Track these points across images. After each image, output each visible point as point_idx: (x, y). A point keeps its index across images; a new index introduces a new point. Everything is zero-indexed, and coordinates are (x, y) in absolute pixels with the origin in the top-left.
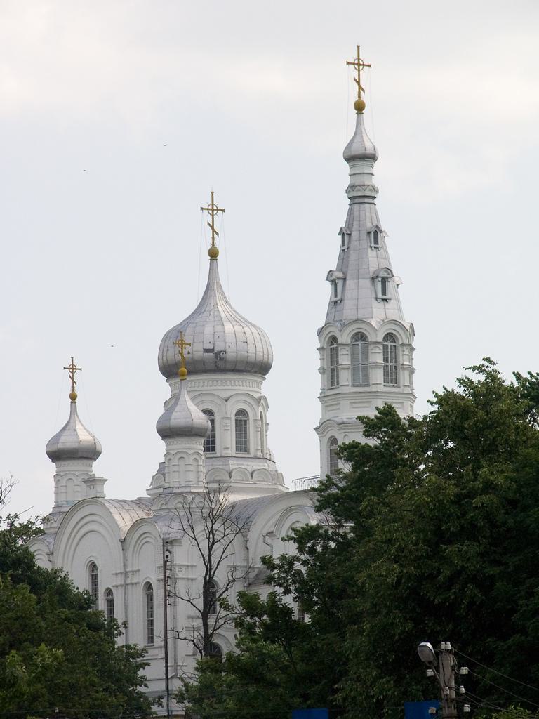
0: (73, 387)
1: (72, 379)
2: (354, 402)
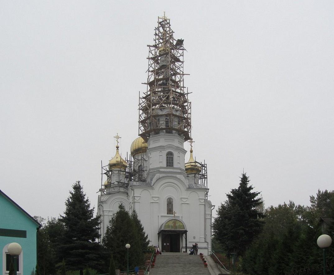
0: (191, 148)
1: (191, 145)
2: (179, 142)
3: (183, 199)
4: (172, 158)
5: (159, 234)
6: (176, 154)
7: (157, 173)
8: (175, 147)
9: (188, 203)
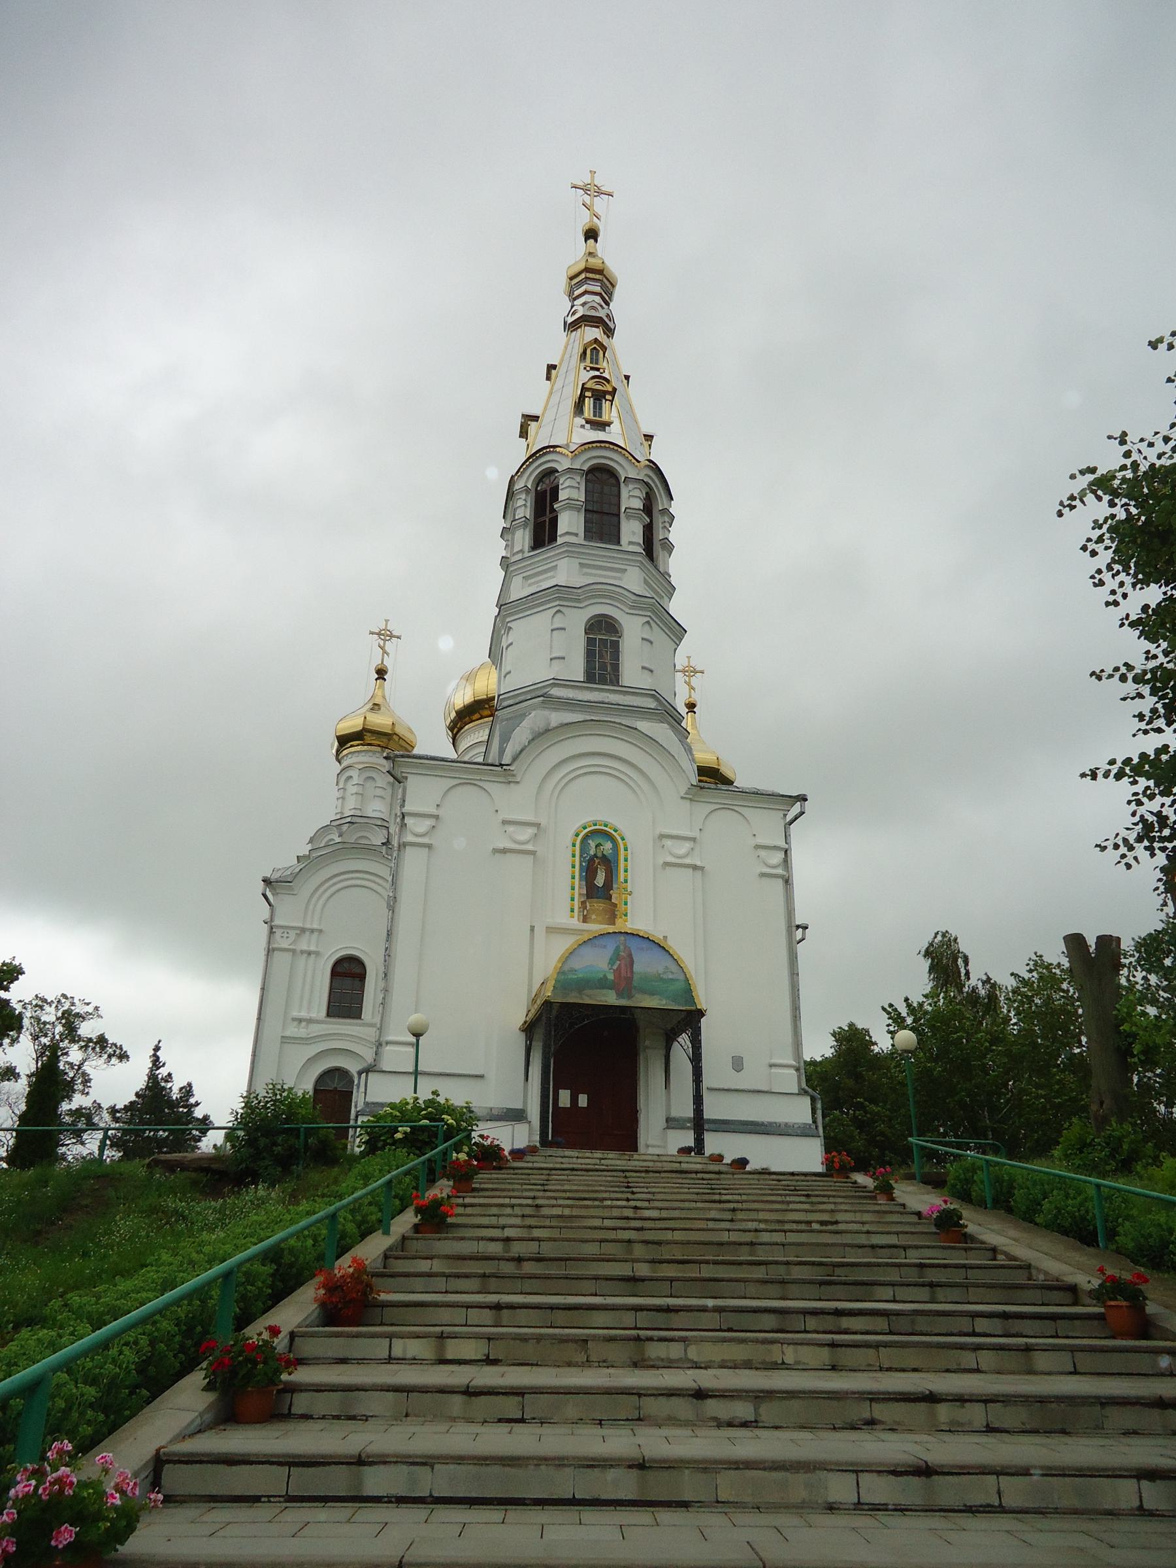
3: (668, 843)
4: (615, 646)
5: (529, 1029)
6: (633, 630)
7: (533, 707)
8: (634, 598)
9: (698, 863)
